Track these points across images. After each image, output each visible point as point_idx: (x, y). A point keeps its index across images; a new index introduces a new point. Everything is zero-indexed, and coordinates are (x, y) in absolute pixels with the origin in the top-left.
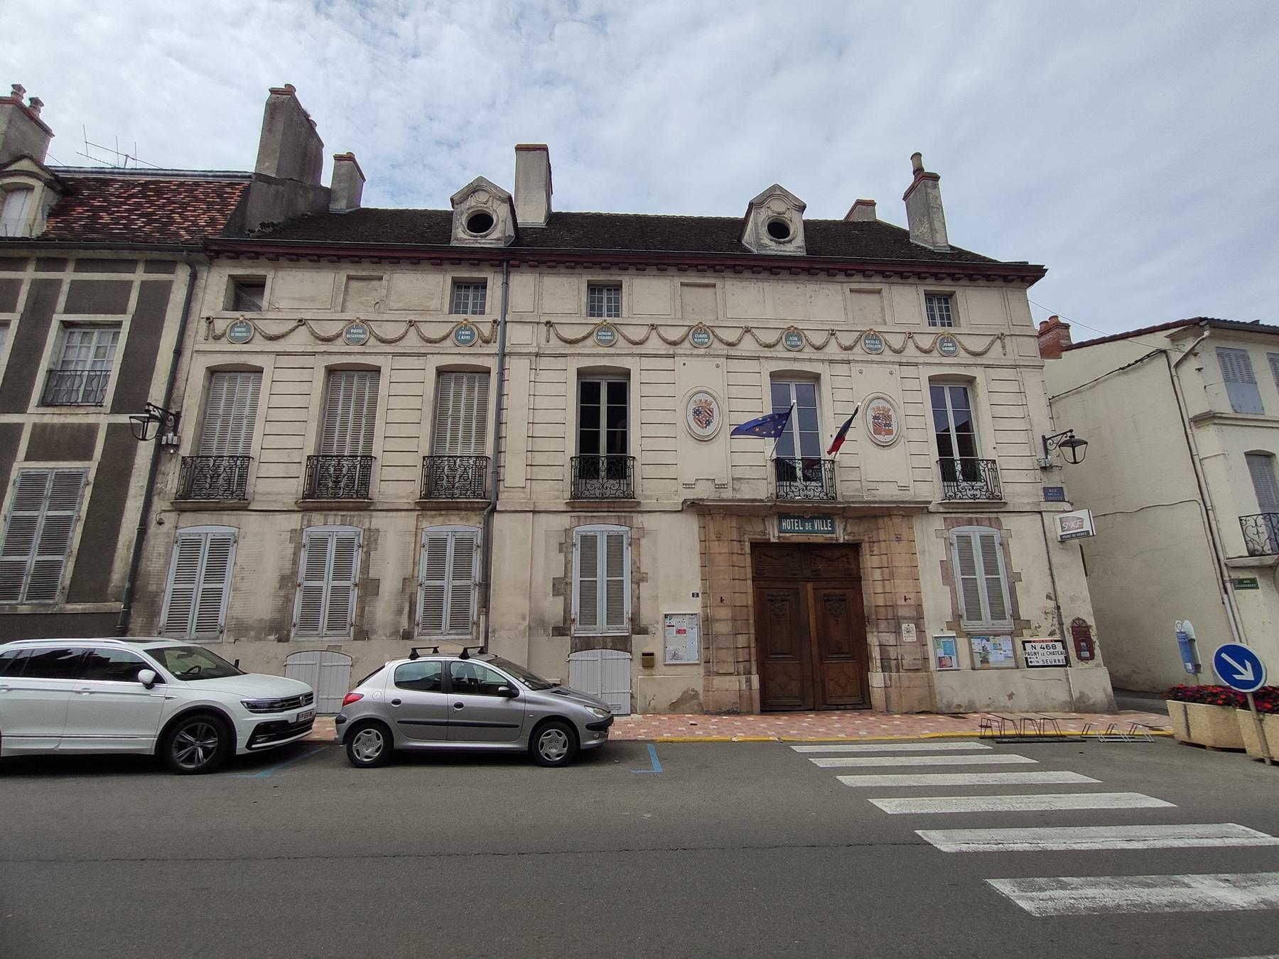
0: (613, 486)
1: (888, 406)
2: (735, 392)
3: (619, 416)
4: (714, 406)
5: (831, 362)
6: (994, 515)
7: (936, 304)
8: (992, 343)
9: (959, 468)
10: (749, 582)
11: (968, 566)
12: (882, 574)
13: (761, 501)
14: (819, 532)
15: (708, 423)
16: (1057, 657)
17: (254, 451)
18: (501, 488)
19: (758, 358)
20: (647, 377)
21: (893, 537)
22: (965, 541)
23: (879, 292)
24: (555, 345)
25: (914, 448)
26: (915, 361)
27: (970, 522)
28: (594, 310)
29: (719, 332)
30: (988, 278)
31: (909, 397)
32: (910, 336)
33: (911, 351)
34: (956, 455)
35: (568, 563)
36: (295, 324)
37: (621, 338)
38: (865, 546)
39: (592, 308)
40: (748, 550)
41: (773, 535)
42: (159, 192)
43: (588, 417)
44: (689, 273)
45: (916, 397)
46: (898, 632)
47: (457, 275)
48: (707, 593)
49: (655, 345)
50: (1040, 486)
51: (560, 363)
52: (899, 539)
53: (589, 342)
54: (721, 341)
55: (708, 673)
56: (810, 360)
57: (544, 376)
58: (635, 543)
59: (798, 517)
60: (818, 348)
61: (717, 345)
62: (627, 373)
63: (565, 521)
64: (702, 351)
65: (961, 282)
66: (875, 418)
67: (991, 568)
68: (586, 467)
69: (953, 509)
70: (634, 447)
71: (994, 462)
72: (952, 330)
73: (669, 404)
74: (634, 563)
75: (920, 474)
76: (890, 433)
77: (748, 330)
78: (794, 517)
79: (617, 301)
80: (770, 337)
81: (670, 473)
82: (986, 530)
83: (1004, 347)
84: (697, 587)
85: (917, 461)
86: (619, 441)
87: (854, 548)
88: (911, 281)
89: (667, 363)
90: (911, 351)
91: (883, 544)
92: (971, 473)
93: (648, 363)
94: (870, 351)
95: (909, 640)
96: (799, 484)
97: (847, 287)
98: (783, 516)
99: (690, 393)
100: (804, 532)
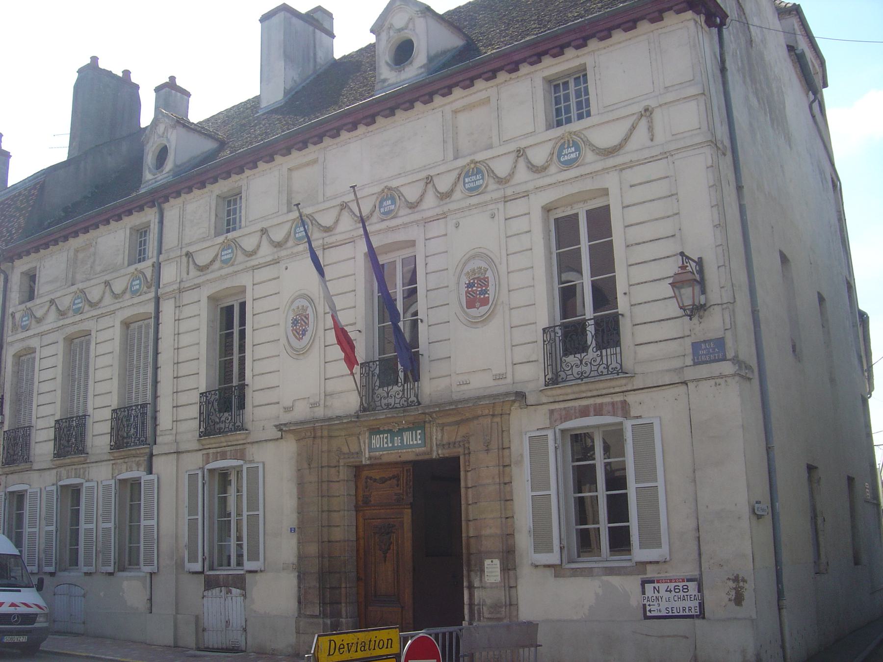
1: (483, 265)
16: (687, 604)
17: (90, 411)
18: (158, 433)
23: (487, 101)
36: (644, 123)
42: (460, 12)
47: (548, 73)
50: (688, 342)
53: (217, 265)
90: (522, 174)
94: (474, 190)
96: (591, 354)
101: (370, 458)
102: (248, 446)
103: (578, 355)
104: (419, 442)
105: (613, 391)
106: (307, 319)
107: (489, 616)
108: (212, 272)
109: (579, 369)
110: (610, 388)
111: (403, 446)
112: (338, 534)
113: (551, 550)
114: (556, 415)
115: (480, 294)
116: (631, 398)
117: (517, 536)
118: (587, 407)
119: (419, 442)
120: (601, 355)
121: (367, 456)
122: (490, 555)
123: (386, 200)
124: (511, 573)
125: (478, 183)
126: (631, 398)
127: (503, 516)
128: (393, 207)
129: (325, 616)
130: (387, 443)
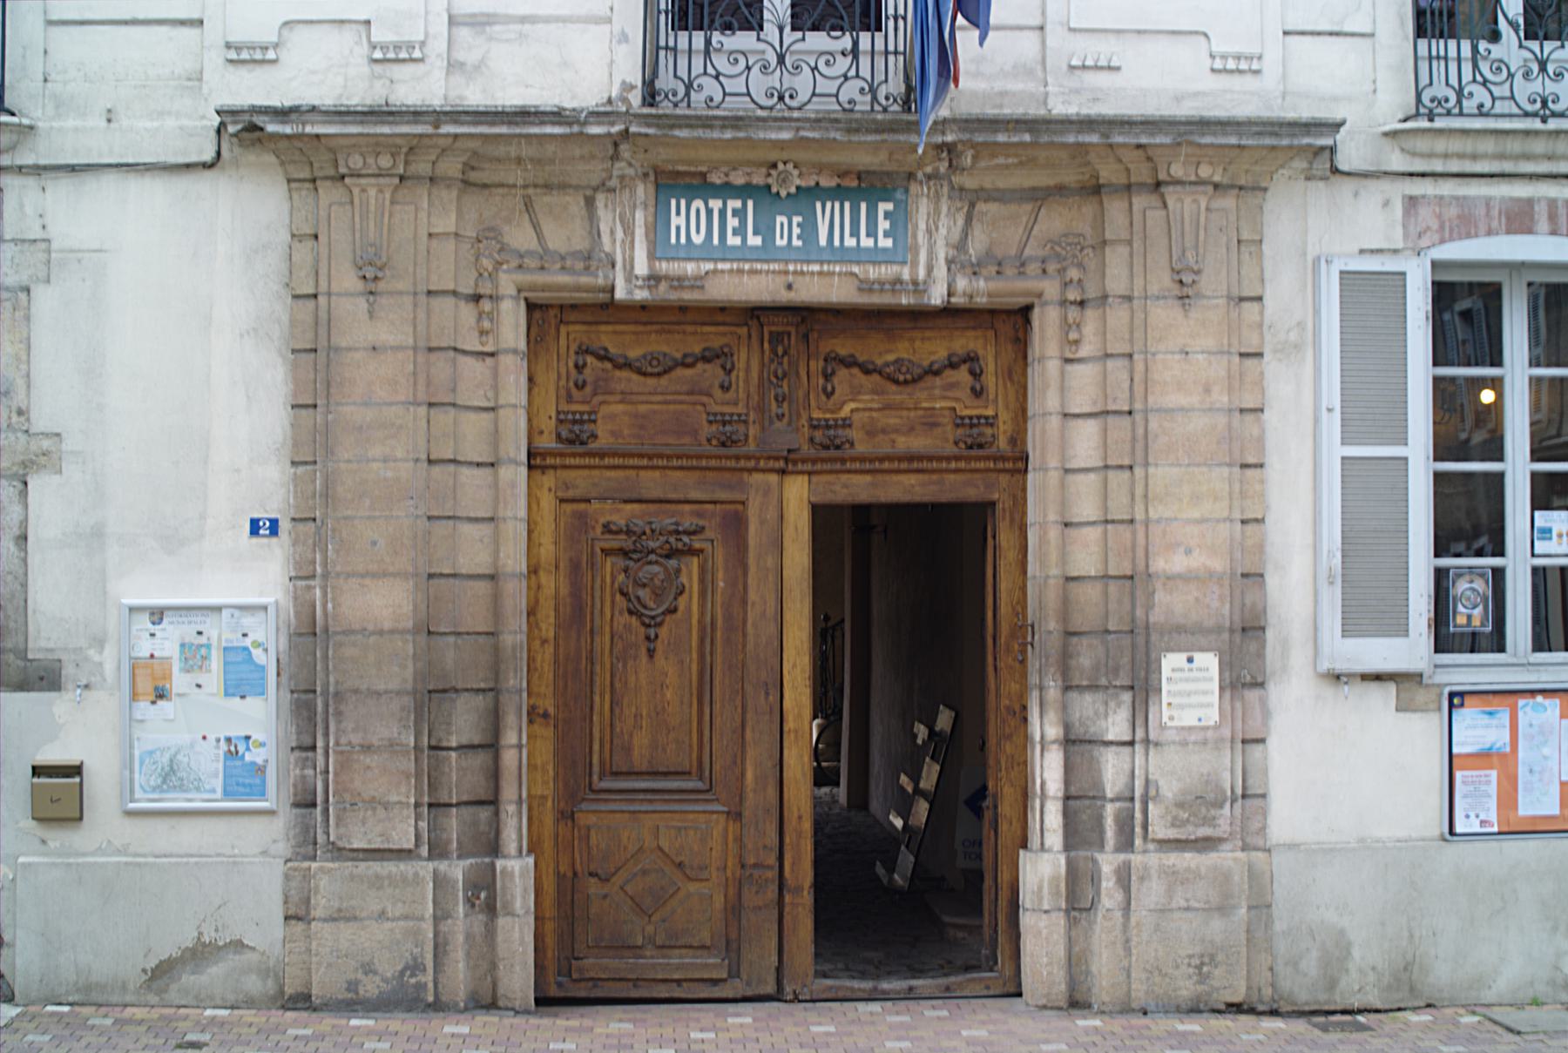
10: (516, 475)
14: (836, 253)
21: (1161, 280)
38: (1046, 327)
40: (512, 327)
46: (1143, 689)
48: (311, 524)
52: (1185, 292)
55: (307, 845)
59: (745, 191)
78: (727, 190)
84: (271, 489)
91: (1118, 316)
95: (1189, 719)
96: (1510, 48)
98: (677, 182)
101: (654, 279)
104: (889, 243)
107: (1172, 834)
112: (471, 551)
113: (1401, 628)
114: (1426, 215)
117: (1271, 581)
120: (855, 52)
121: (641, 268)
122: (1187, 636)
124: (1252, 695)
127: (1237, 515)
129: (438, 851)
130: (740, 231)
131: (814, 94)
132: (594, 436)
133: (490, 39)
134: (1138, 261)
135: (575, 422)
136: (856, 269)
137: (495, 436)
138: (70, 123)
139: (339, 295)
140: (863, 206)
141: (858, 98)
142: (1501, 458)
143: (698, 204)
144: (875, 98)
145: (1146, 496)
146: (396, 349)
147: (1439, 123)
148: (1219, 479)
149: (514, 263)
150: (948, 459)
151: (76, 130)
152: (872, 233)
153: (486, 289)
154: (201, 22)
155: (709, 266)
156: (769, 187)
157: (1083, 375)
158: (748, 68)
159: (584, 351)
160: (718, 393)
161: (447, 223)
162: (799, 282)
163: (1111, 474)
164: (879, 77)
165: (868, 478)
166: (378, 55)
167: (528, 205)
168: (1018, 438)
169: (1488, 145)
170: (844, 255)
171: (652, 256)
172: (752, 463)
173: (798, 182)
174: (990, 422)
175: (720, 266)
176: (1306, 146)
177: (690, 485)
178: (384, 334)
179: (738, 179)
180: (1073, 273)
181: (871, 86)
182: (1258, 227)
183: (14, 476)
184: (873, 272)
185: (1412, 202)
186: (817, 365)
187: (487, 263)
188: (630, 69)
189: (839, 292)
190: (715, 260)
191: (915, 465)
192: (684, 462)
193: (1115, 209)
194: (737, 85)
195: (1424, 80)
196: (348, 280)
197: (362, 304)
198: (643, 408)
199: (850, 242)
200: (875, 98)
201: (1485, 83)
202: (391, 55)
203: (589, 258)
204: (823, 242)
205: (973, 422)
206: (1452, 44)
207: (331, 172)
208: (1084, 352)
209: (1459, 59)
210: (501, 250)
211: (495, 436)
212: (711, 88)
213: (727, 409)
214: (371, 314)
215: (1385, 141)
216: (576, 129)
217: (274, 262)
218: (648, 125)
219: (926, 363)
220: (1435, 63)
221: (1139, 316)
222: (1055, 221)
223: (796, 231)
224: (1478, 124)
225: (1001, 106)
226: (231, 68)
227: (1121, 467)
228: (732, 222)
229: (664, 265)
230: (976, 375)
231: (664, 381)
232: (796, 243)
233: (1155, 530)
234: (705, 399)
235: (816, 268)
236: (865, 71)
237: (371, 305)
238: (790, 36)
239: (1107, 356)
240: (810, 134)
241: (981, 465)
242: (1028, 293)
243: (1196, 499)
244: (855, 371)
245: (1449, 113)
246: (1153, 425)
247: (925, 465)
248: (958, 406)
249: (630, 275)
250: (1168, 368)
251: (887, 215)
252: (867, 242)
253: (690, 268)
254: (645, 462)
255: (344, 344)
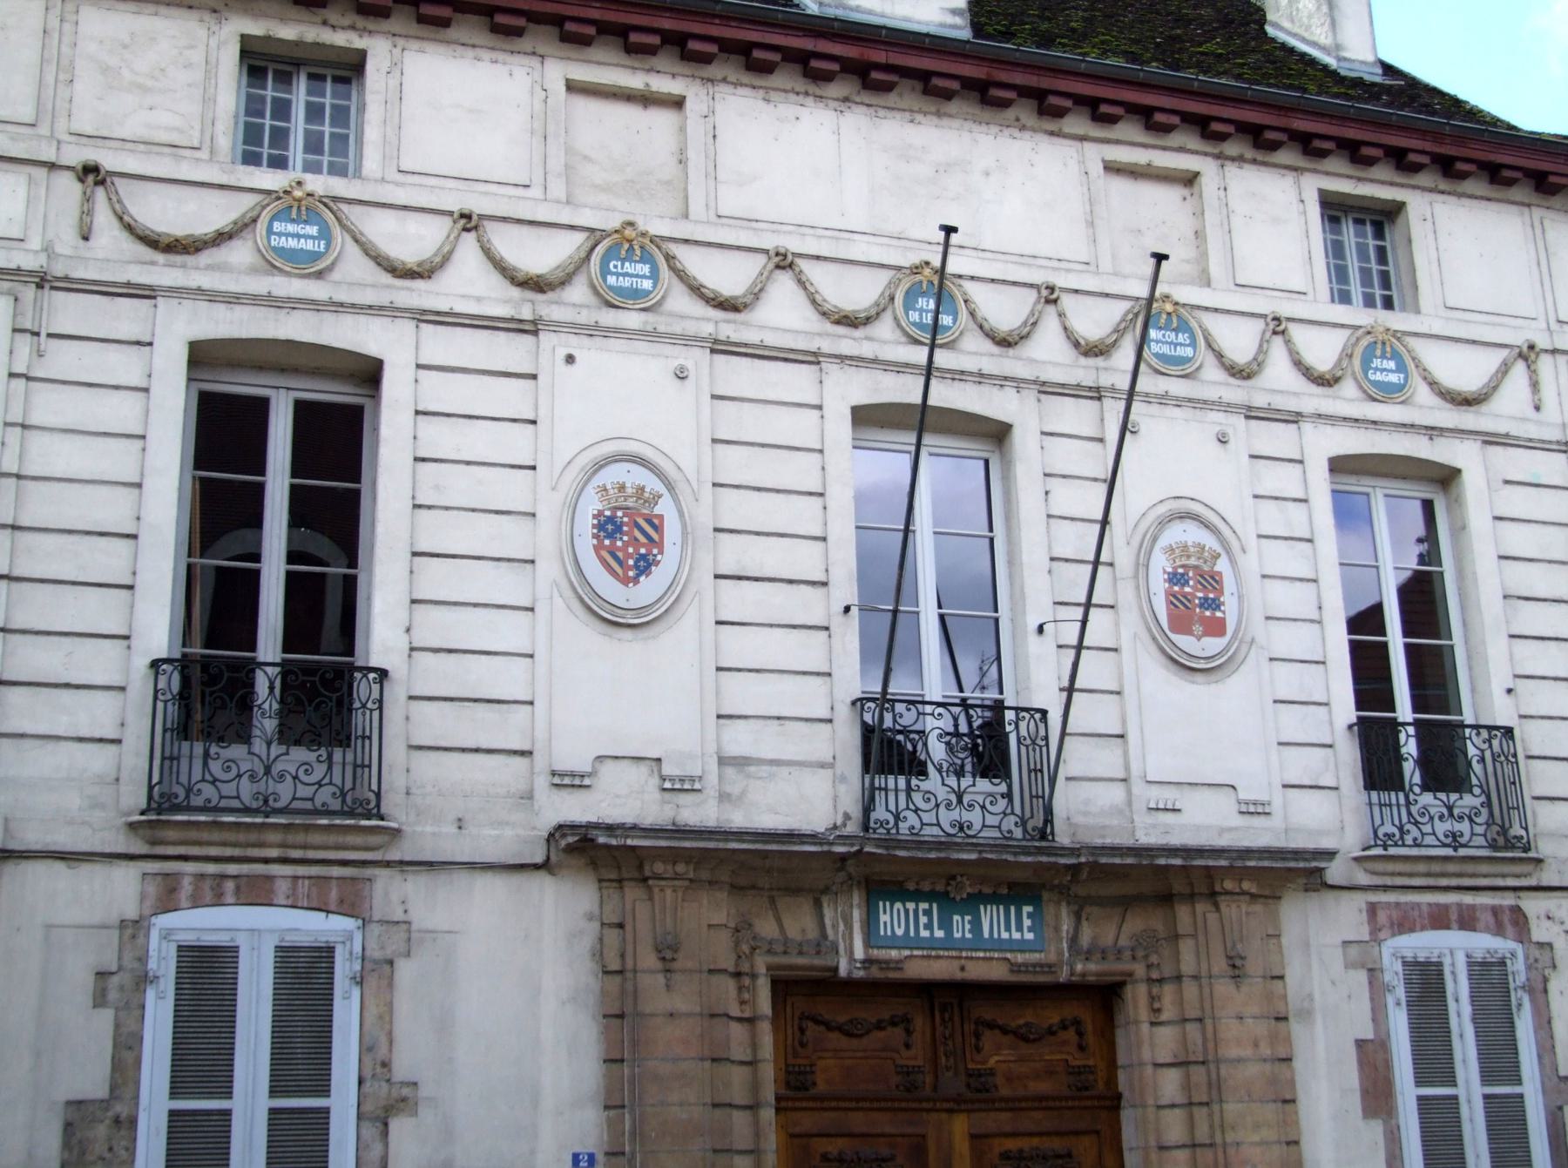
0: (301, 771)
2: (737, 465)
3: (333, 514)
4: (665, 507)
5: (1046, 389)
6: (1507, 900)
7: (1349, 233)
8: (1504, 369)
9: (1410, 747)
11: (1434, 1060)
12: (1187, 1086)
13: (813, 838)
15: (645, 565)
19: (813, 358)
20: (443, 392)
21: (1220, 965)
22: (1426, 983)
23: (1189, 180)
24: (112, 254)
25: (1289, 681)
26: (1292, 405)
27: (1439, 920)
28: (260, 142)
29: (692, 260)
30: (1496, 175)
31: (1274, 519)
32: (1278, 326)
33: (1279, 373)
34: (1404, 710)
35: (127, 1048)
37: (353, 250)
38: (1136, 998)
39: (252, 135)
40: (765, 1004)
41: (852, 953)
43: (221, 510)
44: (595, 52)
45: (1294, 520)
49: (468, 283)
51: (125, 317)
53: (239, 253)
54: (697, 290)
56: (981, 377)
57: (65, 360)
58: (377, 972)
59: (930, 896)
60: (1005, 342)
61: (680, 300)
62: (369, 373)
63: (122, 889)
64: (632, 320)
65: (1424, 179)
66: (1175, 578)
67: (1499, 1060)
68: (204, 694)
69: (1400, 880)
70: (383, 634)
71: (1508, 732)
72: (1396, 320)
73: (510, 490)
74: (366, 1048)
75: (1303, 765)
76: (1216, 628)
77: (784, 262)
78: (917, 896)
79: (341, 116)
80: (857, 292)
81: (506, 729)
82: (1483, 943)
83: (1535, 386)
85: (1295, 724)
86: (327, 605)
87: (1105, 996)
88: (1283, 156)
89: (509, 351)
90: (1279, 373)
91: (1190, 990)
92: (1444, 765)
93: (444, 345)
97: (1095, 154)
99: (649, 453)
100: (948, 943)
101: (868, 962)
102: (382, 874)
103: (1442, 796)
104: (1029, 936)
105: (1500, 882)
106: (658, 529)
108: (209, 267)
109: (955, 815)
110: (1495, 876)
111: (978, 942)
115: (1201, 606)
116: (1533, 906)
118: (1446, 908)
119: (1029, 936)
121: (859, 953)
123: (923, 294)
125: (1180, 351)
126: (1533, 906)
128: (647, 284)
130: (929, 926)
131: (984, 826)
132: (814, 1084)
133: (749, 776)
134: (1202, 950)
135: (800, 1073)
136: (1008, 955)
137: (755, 1087)
138: (429, 829)
139: (644, 971)
140: (1013, 909)
141: (1013, 828)
142: (1420, 1098)
143: (898, 905)
144: (344, 801)
145: (1222, 1126)
146: (689, 1015)
147: (1392, 851)
148: (1269, 1112)
149: (766, 948)
150: (1067, 1099)
151: (434, 834)
152: (1020, 928)
153: (745, 967)
154: (531, 753)
155: (907, 953)
156: (947, 893)
157: (1166, 1035)
158: (937, 806)
159: (803, 1017)
160: (903, 1049)
161: (720, 917)
162: (969, 965)
163: (1195, 1109)
164: (1028, 814)
165: (1009, 1115)
166: (668, 785)
167: (772, 900)
168: (1112, 1080)
169: (1421, 867)
170: (1001, 946)
171: (868, 944)
172: (930, 1105)
173: (969, 890)
174: (1091, 1070)
175: (916, 953)
176: (1296, 872)
177: (885, 1123)
178: (680, 1003)
179: (926, 886)
180: (1154, 959)
181: (342, 790)
182: (1277, 926)
183: (377, 1119)
184: (1020, 958)
185: (1372, 909)
186: (969, 1027)
187: (745, 948)
188: (850, 801)
189: (996, 972)
190: (912, 949)
191: (1044, 1104)
192: (883, 1104)
193: (1183, 913)
194: (928, 818)
195: (1378, 821)
196: (649, 960)
197: (661, 979)
198: (849, 1062)
199: (1005, 935)
200: (344, 801)
201: (916, 811)
202: (678, 786)
203: (822, 944)
204: (986, 935)
205: (1077, 1072)
206: (891, 779)
207: (636, 875)
208: (1164, 1017)
209: (896, 790)
210: (754, 938)
211: (755, 1087)
212: (912, 819)
213: (912, 1063)
214: (668, 986)
215: (1354, 864)
216: (826, 848)
217: (587, 943)
218: (878, 847)
219: (1046, 1026)
220: (359, 770)
221: (1206, 990)
222: (1135, 924)
223: (968, 927)
224: (1415, 852)
225: (1103, 837)
226: (555, 790)
227: (1201, 1104)
228: (923, 920)
229: (875, 951)
230: (909, 1032)
231: (865, 1040)
232: (968, 936)
233: (1231, 1151)
234: (895, 1055)
235: (981, 954)
236: (337, 780)
237: (668, 980)
238: (276, 750)
239: (1186, 1020)
240: (989, 856)
241: (1089, 1103)
242: (1123, 974)
243: (1257, 1127)
244: (997, 1032)
245: (1396, 845)
246: (1223, 1072)
247: (1051, 1104)
248: (1070, 1058)
249: (852, 959)
250: (1230, 1029)
251: (1030, 915)
252: (1016, 936)
253: (894, 953)
254: (853, 1104)
255: (648, 1011)
